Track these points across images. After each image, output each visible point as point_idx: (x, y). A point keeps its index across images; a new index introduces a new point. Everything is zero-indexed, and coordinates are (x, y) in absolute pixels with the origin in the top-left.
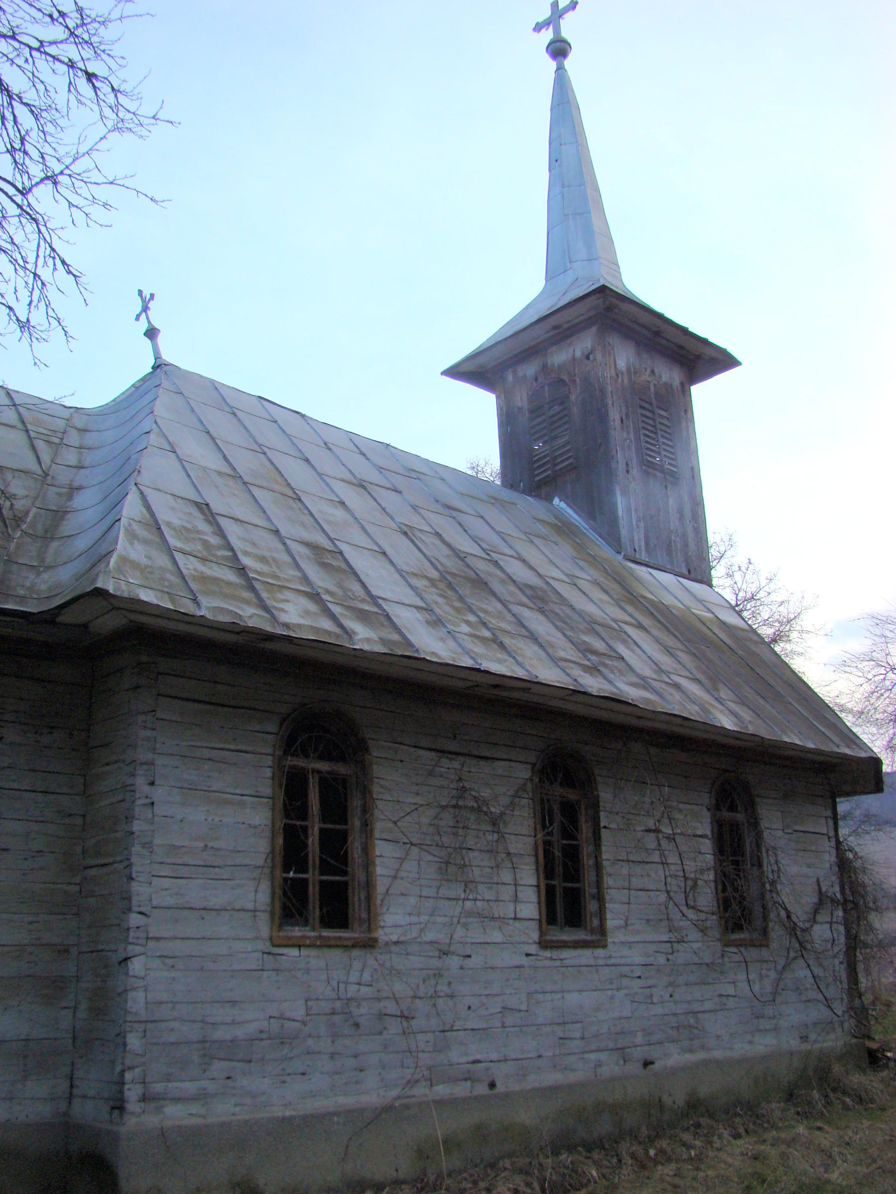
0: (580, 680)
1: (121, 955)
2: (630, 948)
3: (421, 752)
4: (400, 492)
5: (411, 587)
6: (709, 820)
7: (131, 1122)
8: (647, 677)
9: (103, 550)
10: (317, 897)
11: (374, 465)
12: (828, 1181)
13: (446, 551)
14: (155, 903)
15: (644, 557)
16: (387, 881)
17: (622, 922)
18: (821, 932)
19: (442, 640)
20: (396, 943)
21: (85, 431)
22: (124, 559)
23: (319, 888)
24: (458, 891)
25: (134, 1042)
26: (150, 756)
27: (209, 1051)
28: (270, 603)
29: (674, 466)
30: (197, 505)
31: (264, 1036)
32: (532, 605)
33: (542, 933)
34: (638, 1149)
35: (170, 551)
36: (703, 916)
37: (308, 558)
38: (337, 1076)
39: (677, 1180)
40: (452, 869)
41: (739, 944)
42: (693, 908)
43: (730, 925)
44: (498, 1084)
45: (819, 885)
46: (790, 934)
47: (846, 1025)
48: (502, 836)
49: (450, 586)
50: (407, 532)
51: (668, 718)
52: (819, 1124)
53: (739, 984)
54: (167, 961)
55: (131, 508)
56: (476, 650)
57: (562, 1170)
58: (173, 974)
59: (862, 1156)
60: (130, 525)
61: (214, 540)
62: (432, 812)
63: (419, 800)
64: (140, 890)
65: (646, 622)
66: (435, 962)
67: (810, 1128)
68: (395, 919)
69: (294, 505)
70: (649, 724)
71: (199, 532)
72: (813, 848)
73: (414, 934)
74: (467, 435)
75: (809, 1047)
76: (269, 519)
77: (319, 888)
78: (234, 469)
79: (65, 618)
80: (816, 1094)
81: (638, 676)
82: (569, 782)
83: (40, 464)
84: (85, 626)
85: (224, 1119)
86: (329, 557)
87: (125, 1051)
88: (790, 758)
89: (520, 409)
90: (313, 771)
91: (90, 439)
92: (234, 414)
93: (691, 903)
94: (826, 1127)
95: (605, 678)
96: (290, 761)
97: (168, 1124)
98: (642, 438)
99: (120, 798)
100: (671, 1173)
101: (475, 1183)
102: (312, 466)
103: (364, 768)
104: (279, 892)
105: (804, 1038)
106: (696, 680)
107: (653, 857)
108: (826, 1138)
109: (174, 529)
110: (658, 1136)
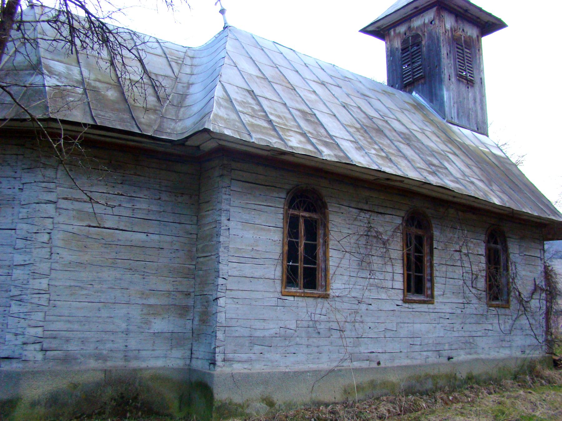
0: (427, 178)
1: (215, 297)
3: (351, 209)
4: (341, 87)
5: (348, 131)
6: (484, 247)
7: (218, 370)
8: (457, 178)
9: (207, 111)
10: (302, 274)
11: (328, 74)
12: (534, 416)
13: (364, 115)
14: (230, 274)
15: (456, 121)
16: (334, 268)
17: (442, 293)
18: (534, 303)
19: (363, 156)
20: (338, 297)
21: (193, 58)
22: (216, 115)
23: (304, 271)
24: (366, 274)
25: (220, 335)
26: (228, 207)
27: (253, 341)
28: (284, 137)
29: (472, 77)
30: (248, 91)
31: (277, 335)
32: (404, 142)
33: (404, 296)
34: (445, 396)
35: (237, 112)
36: (479, 292)
37: (300, 117)
38: (309, 355)
39: (463, 410)
40: (364, 264)
41: (498, 306)
42: (475, 288)
43: (492, 297)
44: (381, 363)
45: (535, 281)
46: (520, 304)
47: (543, 347)
48: (388, 250)
49: (365, 131)
50: (345, 106)
51: (468, 198)
52: (530, 390)
53: (494, 325)
54: (234, 300)
55: (218, 92)
56: (379, 162)
57: (409, 403)
58: (238, 306)
59: (551, 406)
60: (218, 100)
61: (257, 107)
62: (356, 237)
63: (350, 232)
64: (223, 268)
65: (457, 152)
66: (355, 307)
67: (526, 392)
68: (337, 285)
69: (292, 92)
70: (459, 200)
71: (250, 104)
72: (533, 264)
73: (346, 293)
74: (372, 61)
75: (526, 356)
76: (281, 98)
77: (304, 271)
78: (264, 75)
79: (188, 143)
80: (528, 378)
81: (454, 177)
82: (419, 226)
83: (174, 73)
84: (198, 147)
85: (259, 371)
86: (309, 116)
87: (216, 339)
88: (524, 220)
89: (397, 49)
90: (302, 216)
91: (196, 62)
92: (263, 50)
93: (474, 286)
94: (533, 392)
95: (439, 177)
96: (291, 211)
97: (235, 372)
98: (457, 63)
99: (214, 226)
100: (460, 407)
101: (370, 406)
102: (300, 74)
103: (325, 216)
104: (285, 270)
105: (523, 352)
106: (481, 180)
107: (457, 264)
108: (534, 397)
109: (238, 102)
110: (453, 391)
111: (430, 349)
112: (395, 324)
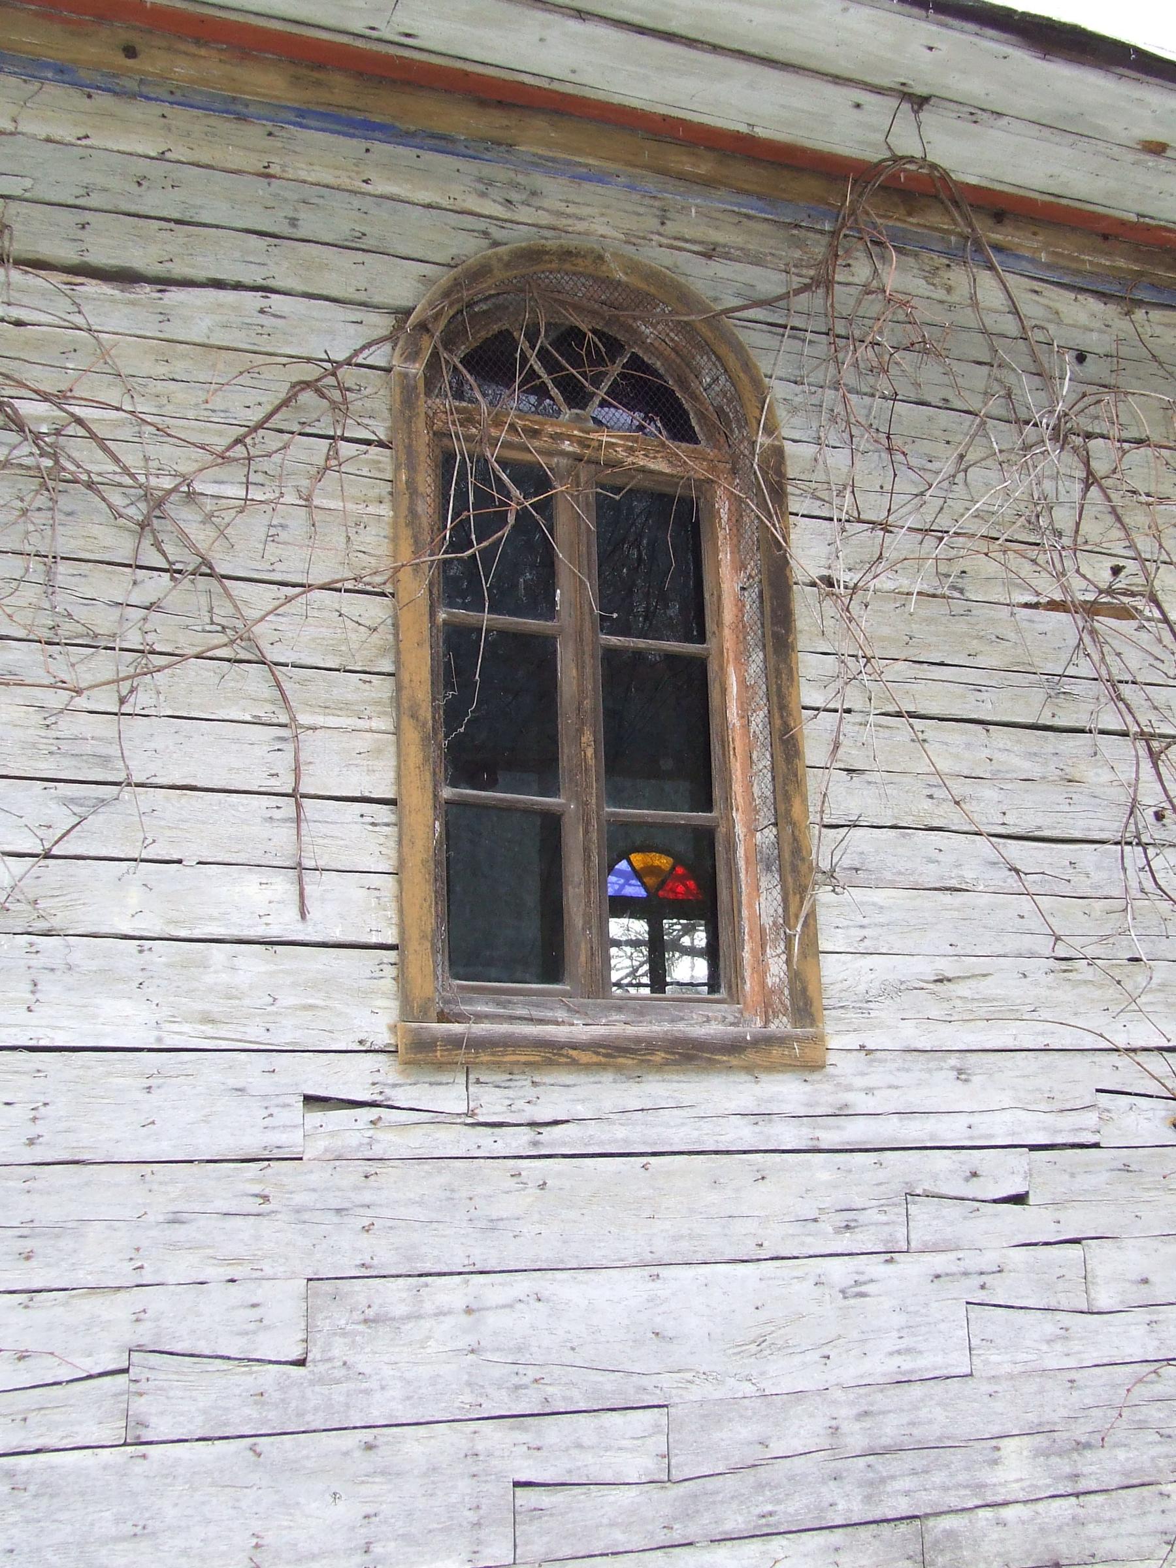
2: (962, 1074)
111: (795, 1508)
112: (283, 1300)
